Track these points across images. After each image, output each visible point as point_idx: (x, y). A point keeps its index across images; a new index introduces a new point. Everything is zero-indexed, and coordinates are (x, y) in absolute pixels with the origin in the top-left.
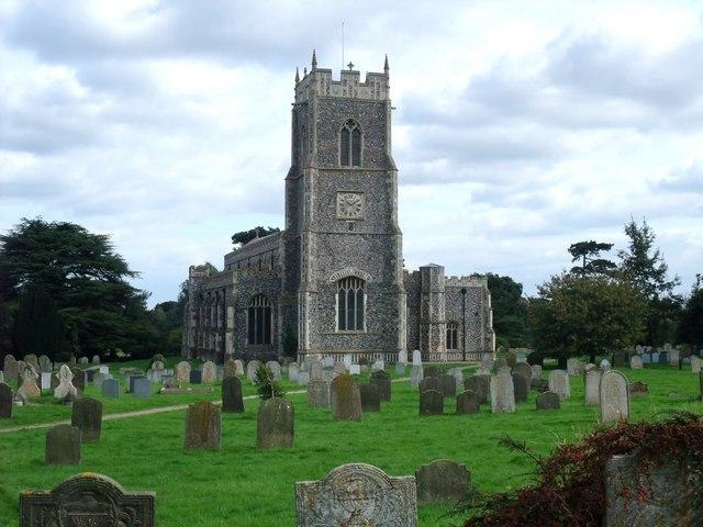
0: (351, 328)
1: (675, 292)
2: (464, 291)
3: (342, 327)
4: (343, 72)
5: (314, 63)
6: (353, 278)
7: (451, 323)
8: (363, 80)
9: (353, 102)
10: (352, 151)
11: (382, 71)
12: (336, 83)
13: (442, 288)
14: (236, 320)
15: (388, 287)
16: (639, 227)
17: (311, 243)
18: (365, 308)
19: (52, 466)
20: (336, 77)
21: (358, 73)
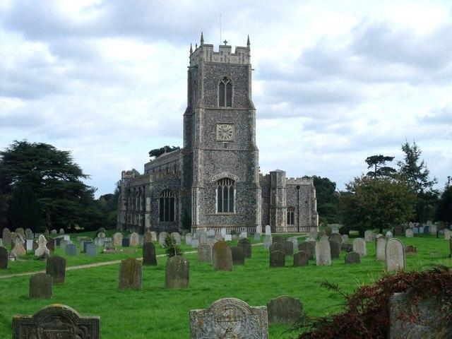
0: (226, 211)
1: (434, 188)
2: (298, 187)
3: (220, 210)
4: (221, 47)
5: (202, 41)
6: (227, 179)
7: (290, 208)
8: (233, 51)
9: (227, 65)
10: (226, 97)
11: (246, 46)
12: (216, 53)
13: (284, 185)
14: (152, 206)
15: (249, 184)
16: (411, 146)
17: (200, 156)
18: (235, 198)
19: (34, 300)
20: (216, 49)
21: (230, 47)
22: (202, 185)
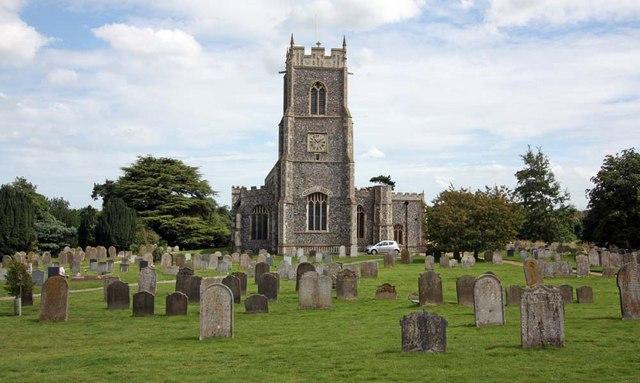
0: (318, 229)
1: (566, 203)
2: (407, 203)
3: (311, 228)
6: (319, 193)
7: (397, 226)
8: (328, 53)
10: (319, 103)
11: (341, 47)
12: (308, 57)
13: (390, 201)
15: (344, 200)
16: (535, 153)
17: (288, 169)
18: (328, 214)
19: (250, 316)
20: (328, 53)
21: (323, 50)
22: (291, 201)
